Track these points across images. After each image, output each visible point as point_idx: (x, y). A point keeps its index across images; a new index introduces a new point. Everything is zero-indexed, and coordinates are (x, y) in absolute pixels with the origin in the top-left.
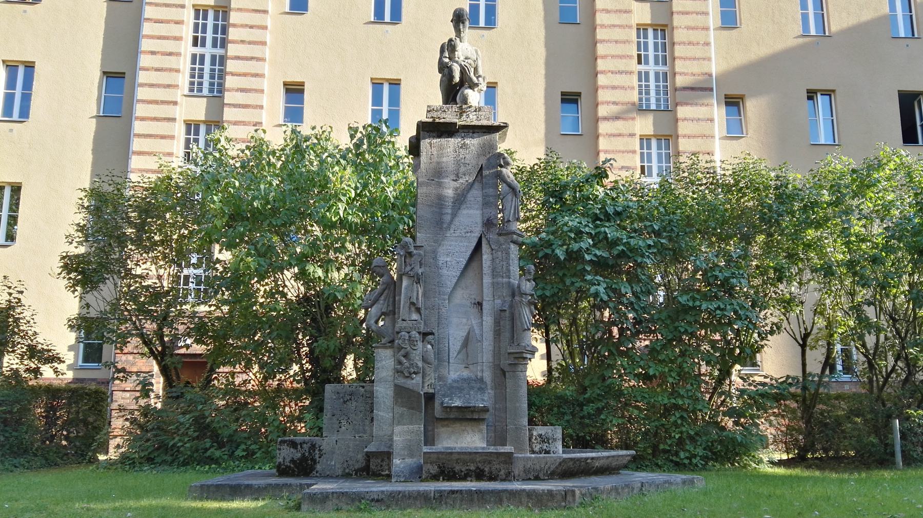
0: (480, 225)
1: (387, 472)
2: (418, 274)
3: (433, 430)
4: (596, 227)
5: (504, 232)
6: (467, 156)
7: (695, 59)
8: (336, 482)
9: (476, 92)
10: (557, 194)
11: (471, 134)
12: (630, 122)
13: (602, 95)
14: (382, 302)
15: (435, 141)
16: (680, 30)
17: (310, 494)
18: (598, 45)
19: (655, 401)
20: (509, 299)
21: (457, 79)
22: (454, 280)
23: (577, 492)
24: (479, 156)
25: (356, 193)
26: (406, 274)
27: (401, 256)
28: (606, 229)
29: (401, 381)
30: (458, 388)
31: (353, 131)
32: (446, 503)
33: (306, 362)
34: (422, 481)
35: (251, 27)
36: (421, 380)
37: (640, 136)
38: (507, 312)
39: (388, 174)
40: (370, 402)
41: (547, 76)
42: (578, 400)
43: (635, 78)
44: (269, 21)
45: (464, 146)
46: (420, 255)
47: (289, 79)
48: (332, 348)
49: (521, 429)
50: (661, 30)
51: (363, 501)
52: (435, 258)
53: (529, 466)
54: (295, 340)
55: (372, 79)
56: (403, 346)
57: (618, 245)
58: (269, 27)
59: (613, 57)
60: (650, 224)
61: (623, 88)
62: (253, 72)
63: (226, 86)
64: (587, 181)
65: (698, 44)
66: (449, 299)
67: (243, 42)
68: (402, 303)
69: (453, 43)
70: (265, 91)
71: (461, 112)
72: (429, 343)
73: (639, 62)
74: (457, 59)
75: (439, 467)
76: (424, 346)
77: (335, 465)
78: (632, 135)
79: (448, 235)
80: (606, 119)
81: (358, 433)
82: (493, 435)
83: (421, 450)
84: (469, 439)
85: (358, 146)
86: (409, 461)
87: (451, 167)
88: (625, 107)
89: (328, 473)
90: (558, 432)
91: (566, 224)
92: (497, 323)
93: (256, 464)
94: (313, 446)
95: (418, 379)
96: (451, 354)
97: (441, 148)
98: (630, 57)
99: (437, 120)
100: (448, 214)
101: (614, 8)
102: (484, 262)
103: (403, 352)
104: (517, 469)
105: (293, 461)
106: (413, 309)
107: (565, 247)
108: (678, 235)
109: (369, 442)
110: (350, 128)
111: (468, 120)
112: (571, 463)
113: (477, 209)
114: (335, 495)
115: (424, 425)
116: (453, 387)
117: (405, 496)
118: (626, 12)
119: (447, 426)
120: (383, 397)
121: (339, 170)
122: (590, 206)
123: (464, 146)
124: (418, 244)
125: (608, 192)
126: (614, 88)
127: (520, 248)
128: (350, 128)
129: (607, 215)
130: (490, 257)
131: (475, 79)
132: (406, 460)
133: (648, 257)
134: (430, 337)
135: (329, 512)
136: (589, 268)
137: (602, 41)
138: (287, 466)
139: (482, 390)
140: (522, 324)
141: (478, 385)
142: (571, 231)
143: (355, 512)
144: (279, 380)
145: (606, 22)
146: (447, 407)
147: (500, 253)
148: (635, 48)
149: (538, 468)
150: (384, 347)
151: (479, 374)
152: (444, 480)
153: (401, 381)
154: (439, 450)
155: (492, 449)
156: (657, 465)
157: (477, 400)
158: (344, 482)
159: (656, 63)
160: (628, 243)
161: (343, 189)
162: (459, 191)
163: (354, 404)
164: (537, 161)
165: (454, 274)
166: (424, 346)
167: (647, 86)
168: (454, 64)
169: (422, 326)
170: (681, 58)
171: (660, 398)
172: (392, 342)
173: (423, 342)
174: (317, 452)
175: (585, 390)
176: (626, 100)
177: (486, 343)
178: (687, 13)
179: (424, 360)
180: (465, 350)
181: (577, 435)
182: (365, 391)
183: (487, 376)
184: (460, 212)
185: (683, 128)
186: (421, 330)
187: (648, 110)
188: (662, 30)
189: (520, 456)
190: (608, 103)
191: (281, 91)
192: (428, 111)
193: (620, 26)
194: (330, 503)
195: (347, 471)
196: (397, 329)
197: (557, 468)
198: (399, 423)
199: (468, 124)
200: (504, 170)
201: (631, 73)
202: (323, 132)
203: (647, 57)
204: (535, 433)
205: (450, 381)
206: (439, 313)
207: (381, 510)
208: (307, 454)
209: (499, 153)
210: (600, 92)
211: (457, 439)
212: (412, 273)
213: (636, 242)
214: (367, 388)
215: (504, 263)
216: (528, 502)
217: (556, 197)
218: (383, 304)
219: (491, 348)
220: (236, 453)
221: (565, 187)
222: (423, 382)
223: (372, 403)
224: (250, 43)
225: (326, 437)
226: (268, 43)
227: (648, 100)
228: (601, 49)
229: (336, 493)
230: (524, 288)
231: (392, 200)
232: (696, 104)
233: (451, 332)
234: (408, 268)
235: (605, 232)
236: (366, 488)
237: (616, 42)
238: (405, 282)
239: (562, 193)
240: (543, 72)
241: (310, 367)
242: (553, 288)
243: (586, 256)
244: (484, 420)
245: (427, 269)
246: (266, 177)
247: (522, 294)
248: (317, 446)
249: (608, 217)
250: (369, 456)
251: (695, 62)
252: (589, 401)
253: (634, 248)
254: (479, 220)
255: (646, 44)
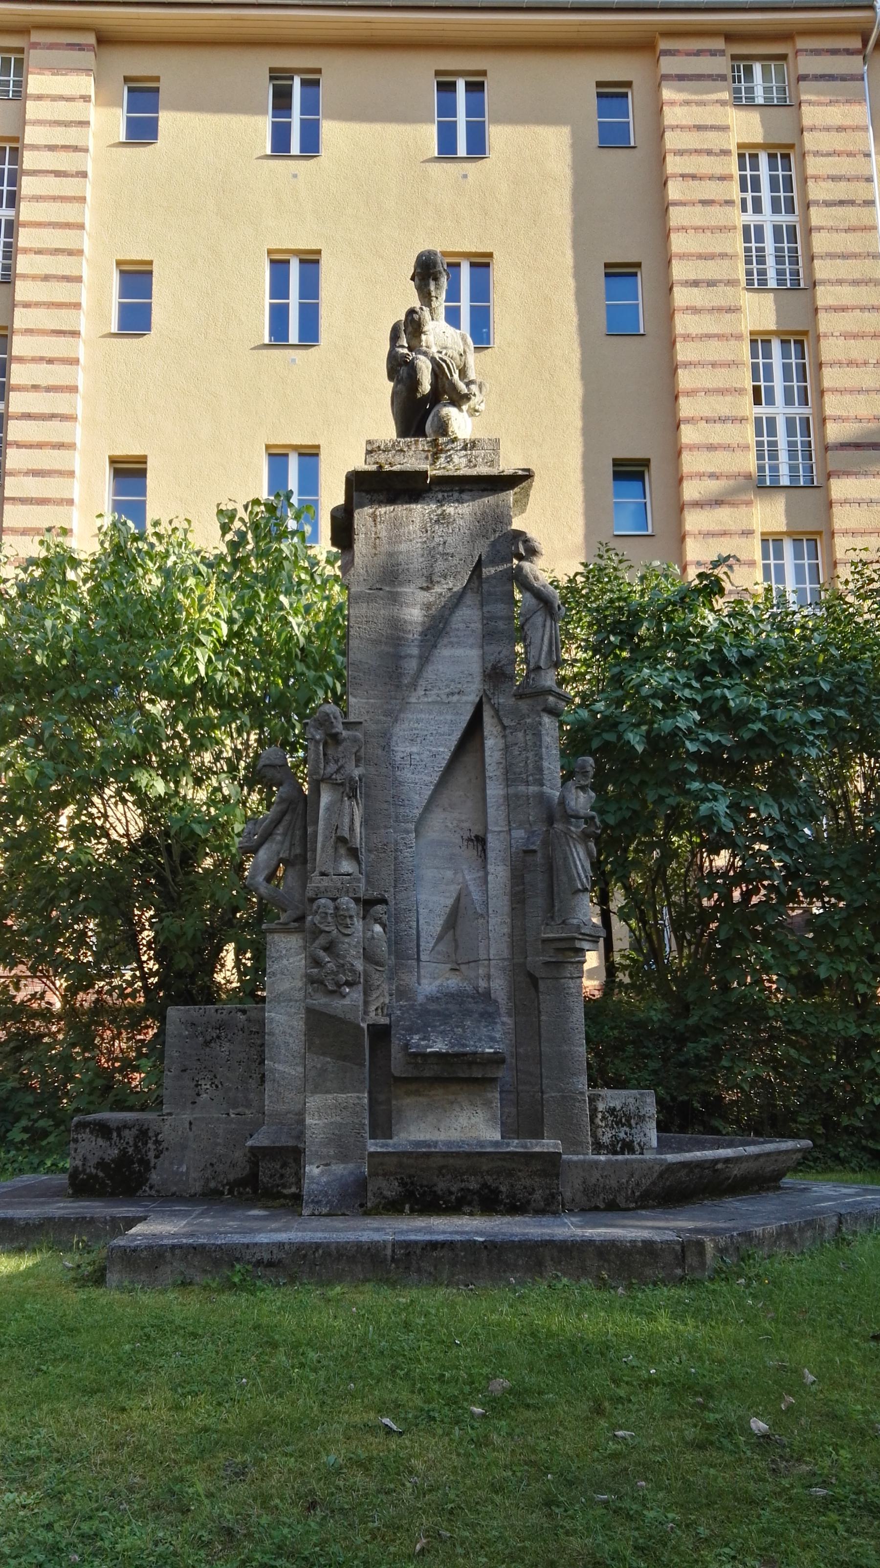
0: (478, 678)
1: (293, 1190)
2: (351, 779)
3: (389, 1101)
4: (706, 687)
5: (528, 691)
6: (449, 540)
7: (860, 391)
8: (185, 1215)
9: (465, 413)
10: (623, 627)
11: (456, 495)
12: (743, 509)
13: (690, 462)
14: (279, 838)
15: (383, 510)
16: (831, 340)
17: (123, 1249)
18: (680, 371)
19: (830, 1029)
20: (543, 828)
21: (426, 386)
22: (427, 792)
23: (710, 1246)
24: (473, 538)
25: (230, 630)
26: (328, 779)
27: (317, 742)
28: (726, 691)
29: (320, 1001)
30: (438, 1013)
31: (226, 518)
32: (419, 1271)
33: (150, 959)
34: (367, 1213)
35: (50, 361)
36: (362, 998)
37: (763, 534)
38: (539, 855)
39: (295, 590)
40: (259, 1042)
41: (586, 431)
42: (674, 1030)
43: (750, 429)
44: (81, 351)
45: (442, 520)
46: (355, 740)
47: (119, 452)
48: (190, 933)
49: (574, 1099)
50: (796, 342)
51: (238, 1267)
52: (387, 747)
53: (594, 1181)
54: (128, 919)
55: (268, 447)
56: (322, 926)
57: (753, 722)
58: (82, 361)
59: (707, 392)
60: (811, 679)
61: (727, 447)
62: (55, 439)
63: (7, 467)
64: (682, 599)
65: (865, 363)
66: (416, 831)
67: (35, 387)
68: (320, 839)
69: (416, 317)
70: (77, 474)
71: (436, 452)
72: (378, 921)
73: (757, 401)
74: (424, 349)
75: (403, 1184)
76: (367, 928)
77: (187, 1172)
78: (747, 533)
79: (413, 700)
80: (698, 504)
81: (234, 1105)
82: (514, 1110)
83: (364, 1148)
84: (463, 1120)
85: (234, 546)
86: (339, 1169)
87: (417, 563)
88: (732, 482)
89: (174, 1189)
90: (651, 1108)
91: (646, 681)
92: (518, 876)
93: (48, 1156)
94: (143, 1134)
95: (354, 996)
96: (422, 944)
97: (396, 524)
98: (740, 391)
99: (387, 468)
100: (411, 656)
101: (708, 305)
102: (487, 753)
103: (322, 940)
104: (569, 1189)
105: (101, 1164)
106: (342, 851)
107: (644, 728)
108: (868, 700)
109: (256, 1126)
110: (220, 512)
111: (451, 467)
112: (683, 1173)
113: (472, 647)
114: (177, 1251)
115: (370, 1093)
116: (428, 1012)
117: (330, 1255)
118: (730, 310)
119: (417, 1093)
120: (284, 1032)
121: (197, 585)
122: (690, 648)
123: (442, 520)
124: (352, 718)
125: (726, 620)
126: (711, 448)
127: (561, 727)
128: (220, 512)
129: (724, 662)
130: (501, 743)
131: (462, 387)
132: (334, 1167)
133: (813, 744)
134: (380, 908)
135: (164, 1292)
136: (693, 769)
137: (687, 365)
138: (91, 1176)
139: (489, 1017)
140: (571, 879)
141: (481, 1007)
142: (654, 696)
143: (221, 1290)
144: (99, 992)
145: (694, 330)
146: (415, 1055)
147: (520, 735)
148: (749, 374)
149: (613, 1183)
150: (285, 929)
151: (483, 984)
152: (412, 1211)
153: (320, 1001)
154: (400, 1149)
155: (514, 1146)
156: (836, 1157)
157: (480, 1040)
158: (202, 1214)
159: (789, 401)
160: (772, 719)
161: (206, 621)
162: (433, 611)
163: (226, 1046)
164: (581, 569)
165: (427, 779)
166: (367, 928)
167: (773, 444)
168: (421, 357)
169: (362, 885)
170: (835, 390)
171: (840, 1025)
172: (301, 919)
173: (364, 918)
174: (150, 1145)
175: (686, 1009)
176: (735, 469)
177: (493, 921)
178: (844, 309)
179: (369, 957)
180: (451, 932)
181: (674, 1099)
182: (249, 1020)
183: (499, 987)
184: (436, 652)
185: (842, 519)
186: (361, 895)
187: (776, 487)
188: (800, 343)
189: (575, 1158)
190: (701, 475)
191: (106, 473)
192: (369, 452)
193: (719, 337)
194: (168, 1269)
195: (212, 1185)
196: (310, 894)
197: (654, 1183)
198: (316, 1090)
199: (451, 473)
200: (526, 565)
201: (742, 420)
202: (175, 530)
203: (770, 391)
204: (601, 1106)
205: (421, 999)
206: (396, 858)
207: (278, 1285)
208: (130, 1150)
209: (515, 531)
210: (686, 457)
211: (439, 1121)
212: (339, 778)
213: (787, 715)
214: (253, 1014)
215: (531, 755)
216: (600, 1268)
217: (620, 634)
218: (282, 843)
219: (506, 930)
220: (10, 1136)
221: (635, 618)
222: (366, 1003)
223: (263, 1045)
224: (49, 389)
225: (170, 1114)
226: (81, 388)
227: (775, 469)
228: (685, 379)
229: (180, 1247)
230: (573, 803)
231: (302, 641)
232: (866, 474)
233: (422, 897)
234: (332, 767)
235: (724, 697)
236: (244, 1232)
237: (714, 365)
238: (325, 798)
239: (634, 625)
240: (579, 424)
241: (156, 967)
242: (620, 809)
243: (688, 744)
244: (493, 1080)
245: (372, 770)
246: (58, 606)
247: (570, 817)
248: (151, 1134)
249: (728, 669)
250: (257, 1155)
251: (861, 397)
252: (698, 1032)
253: (782, 728)
254: (476, 668)
255: (768, 368)
